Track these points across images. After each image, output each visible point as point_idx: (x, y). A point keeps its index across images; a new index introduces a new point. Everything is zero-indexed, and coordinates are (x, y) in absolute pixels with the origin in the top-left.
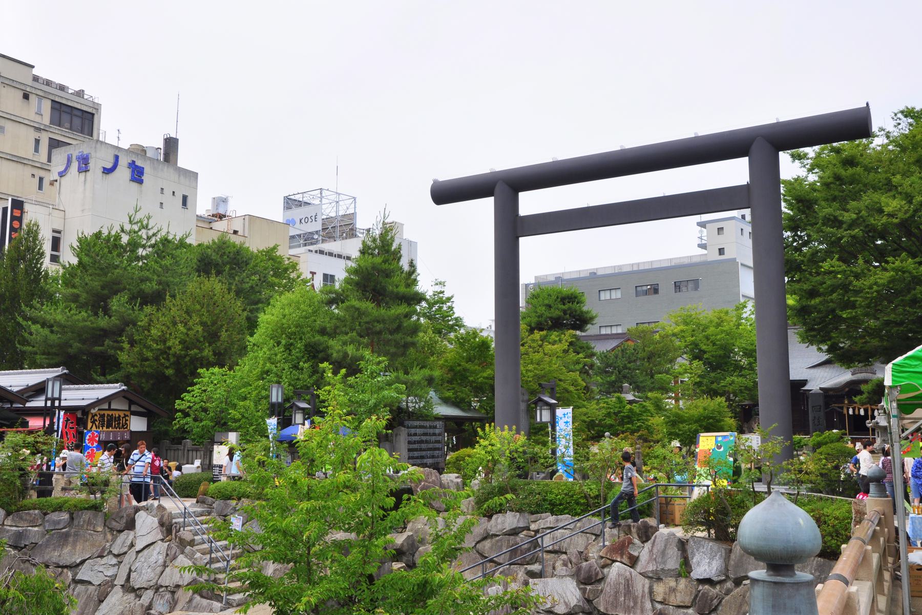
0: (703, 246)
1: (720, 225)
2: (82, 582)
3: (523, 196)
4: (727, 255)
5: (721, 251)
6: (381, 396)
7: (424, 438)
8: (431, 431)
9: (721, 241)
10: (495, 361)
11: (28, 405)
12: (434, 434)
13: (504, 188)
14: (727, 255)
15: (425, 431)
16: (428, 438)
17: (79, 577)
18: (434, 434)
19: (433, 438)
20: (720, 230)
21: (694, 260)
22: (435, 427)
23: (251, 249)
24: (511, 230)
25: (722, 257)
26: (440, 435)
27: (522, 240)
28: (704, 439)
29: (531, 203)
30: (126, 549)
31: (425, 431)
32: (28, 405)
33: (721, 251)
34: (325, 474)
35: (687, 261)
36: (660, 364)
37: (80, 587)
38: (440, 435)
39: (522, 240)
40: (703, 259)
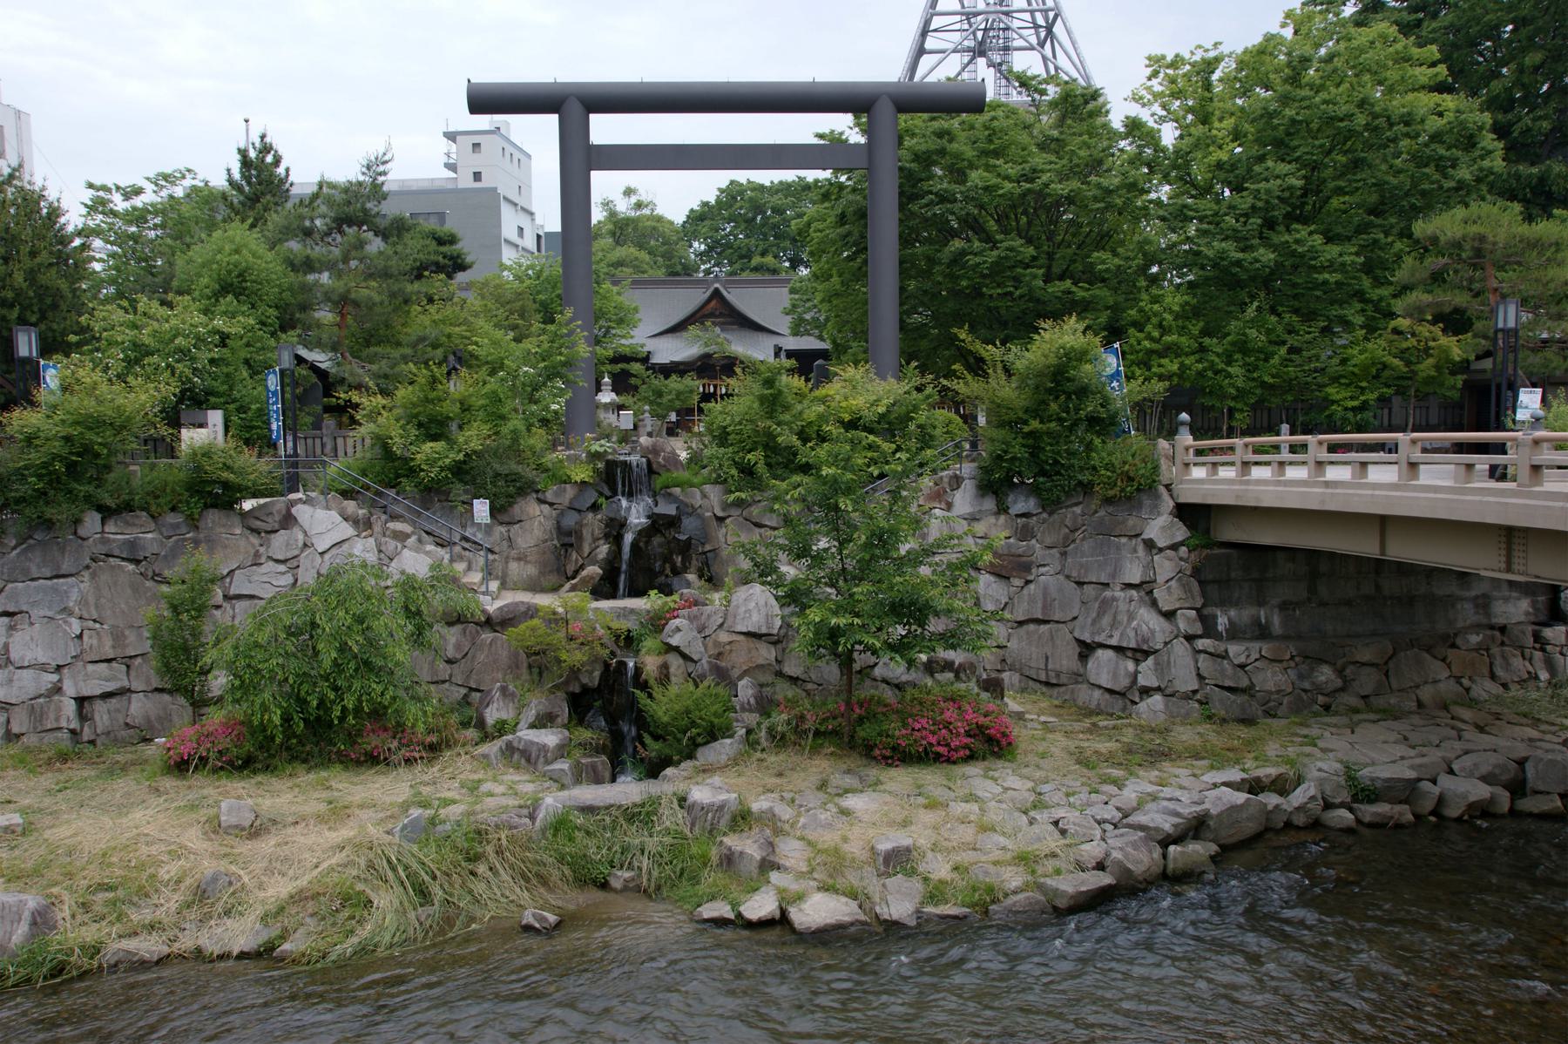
0: (452, 167)
1: (476, 139)
2: (239, 597)
3: (595, 119)
4: (485, 183)
5: (477, 176)
13: (571, 105)
17: (233, 591)
20: (476, 146)
21: (437, 185)
23: (398, 175)
24: (580, 159)
25: (478, 185)
27: (593, 173)
29: (606, 129)
30: (296, 552)
33: (477, 176)
34: (1160, 326)
35: (425, 186)
36: (1495, 244)
37: (240, 605)
39: (593, 173)
40: (450, 186)
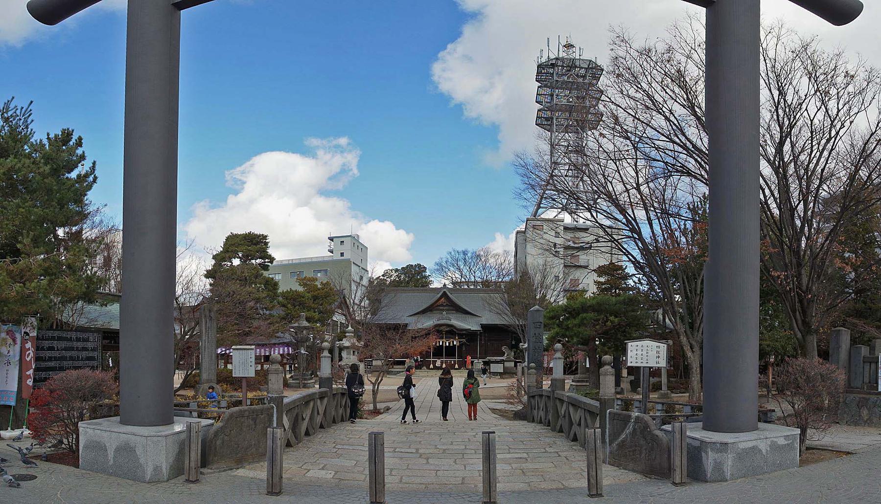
0: (331, 252)
4: (346, 257)
5: (342, 254)
6: (561, 216)
7: (68, 354)
8: (80, 345)
9: (342, 249)
10: (460, 249)
11: (285, 416)
12: (85, 349)
14: (346, 257)
15: (69, 344)
16: (74, 353)
18: (85, 349)
19: (84, 354)
22: (87, 340)
26: (94, 350)
28: (237, 372)
31: (69, 344)
32: (285, 416)
33: (342, 254)
38: (94, 350)
